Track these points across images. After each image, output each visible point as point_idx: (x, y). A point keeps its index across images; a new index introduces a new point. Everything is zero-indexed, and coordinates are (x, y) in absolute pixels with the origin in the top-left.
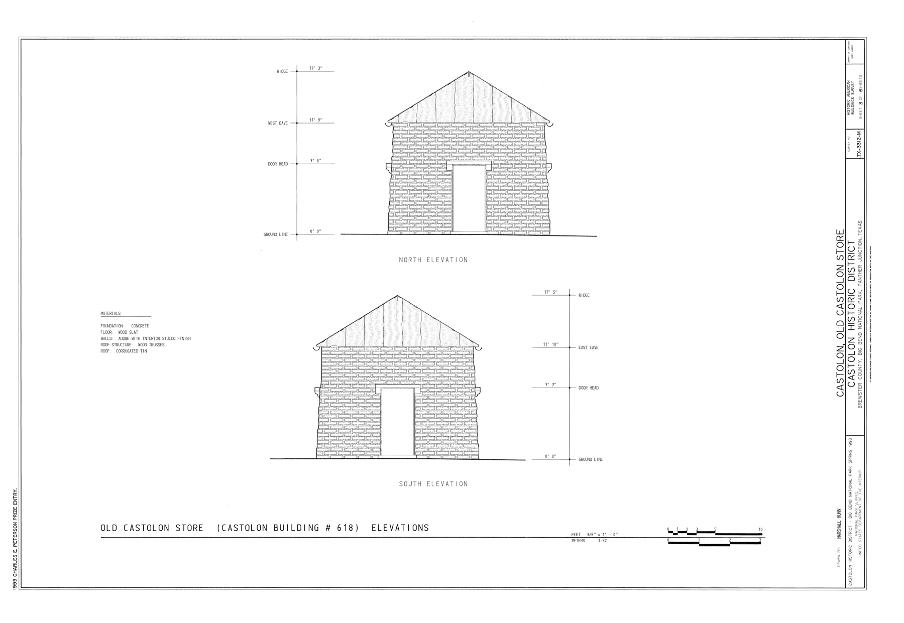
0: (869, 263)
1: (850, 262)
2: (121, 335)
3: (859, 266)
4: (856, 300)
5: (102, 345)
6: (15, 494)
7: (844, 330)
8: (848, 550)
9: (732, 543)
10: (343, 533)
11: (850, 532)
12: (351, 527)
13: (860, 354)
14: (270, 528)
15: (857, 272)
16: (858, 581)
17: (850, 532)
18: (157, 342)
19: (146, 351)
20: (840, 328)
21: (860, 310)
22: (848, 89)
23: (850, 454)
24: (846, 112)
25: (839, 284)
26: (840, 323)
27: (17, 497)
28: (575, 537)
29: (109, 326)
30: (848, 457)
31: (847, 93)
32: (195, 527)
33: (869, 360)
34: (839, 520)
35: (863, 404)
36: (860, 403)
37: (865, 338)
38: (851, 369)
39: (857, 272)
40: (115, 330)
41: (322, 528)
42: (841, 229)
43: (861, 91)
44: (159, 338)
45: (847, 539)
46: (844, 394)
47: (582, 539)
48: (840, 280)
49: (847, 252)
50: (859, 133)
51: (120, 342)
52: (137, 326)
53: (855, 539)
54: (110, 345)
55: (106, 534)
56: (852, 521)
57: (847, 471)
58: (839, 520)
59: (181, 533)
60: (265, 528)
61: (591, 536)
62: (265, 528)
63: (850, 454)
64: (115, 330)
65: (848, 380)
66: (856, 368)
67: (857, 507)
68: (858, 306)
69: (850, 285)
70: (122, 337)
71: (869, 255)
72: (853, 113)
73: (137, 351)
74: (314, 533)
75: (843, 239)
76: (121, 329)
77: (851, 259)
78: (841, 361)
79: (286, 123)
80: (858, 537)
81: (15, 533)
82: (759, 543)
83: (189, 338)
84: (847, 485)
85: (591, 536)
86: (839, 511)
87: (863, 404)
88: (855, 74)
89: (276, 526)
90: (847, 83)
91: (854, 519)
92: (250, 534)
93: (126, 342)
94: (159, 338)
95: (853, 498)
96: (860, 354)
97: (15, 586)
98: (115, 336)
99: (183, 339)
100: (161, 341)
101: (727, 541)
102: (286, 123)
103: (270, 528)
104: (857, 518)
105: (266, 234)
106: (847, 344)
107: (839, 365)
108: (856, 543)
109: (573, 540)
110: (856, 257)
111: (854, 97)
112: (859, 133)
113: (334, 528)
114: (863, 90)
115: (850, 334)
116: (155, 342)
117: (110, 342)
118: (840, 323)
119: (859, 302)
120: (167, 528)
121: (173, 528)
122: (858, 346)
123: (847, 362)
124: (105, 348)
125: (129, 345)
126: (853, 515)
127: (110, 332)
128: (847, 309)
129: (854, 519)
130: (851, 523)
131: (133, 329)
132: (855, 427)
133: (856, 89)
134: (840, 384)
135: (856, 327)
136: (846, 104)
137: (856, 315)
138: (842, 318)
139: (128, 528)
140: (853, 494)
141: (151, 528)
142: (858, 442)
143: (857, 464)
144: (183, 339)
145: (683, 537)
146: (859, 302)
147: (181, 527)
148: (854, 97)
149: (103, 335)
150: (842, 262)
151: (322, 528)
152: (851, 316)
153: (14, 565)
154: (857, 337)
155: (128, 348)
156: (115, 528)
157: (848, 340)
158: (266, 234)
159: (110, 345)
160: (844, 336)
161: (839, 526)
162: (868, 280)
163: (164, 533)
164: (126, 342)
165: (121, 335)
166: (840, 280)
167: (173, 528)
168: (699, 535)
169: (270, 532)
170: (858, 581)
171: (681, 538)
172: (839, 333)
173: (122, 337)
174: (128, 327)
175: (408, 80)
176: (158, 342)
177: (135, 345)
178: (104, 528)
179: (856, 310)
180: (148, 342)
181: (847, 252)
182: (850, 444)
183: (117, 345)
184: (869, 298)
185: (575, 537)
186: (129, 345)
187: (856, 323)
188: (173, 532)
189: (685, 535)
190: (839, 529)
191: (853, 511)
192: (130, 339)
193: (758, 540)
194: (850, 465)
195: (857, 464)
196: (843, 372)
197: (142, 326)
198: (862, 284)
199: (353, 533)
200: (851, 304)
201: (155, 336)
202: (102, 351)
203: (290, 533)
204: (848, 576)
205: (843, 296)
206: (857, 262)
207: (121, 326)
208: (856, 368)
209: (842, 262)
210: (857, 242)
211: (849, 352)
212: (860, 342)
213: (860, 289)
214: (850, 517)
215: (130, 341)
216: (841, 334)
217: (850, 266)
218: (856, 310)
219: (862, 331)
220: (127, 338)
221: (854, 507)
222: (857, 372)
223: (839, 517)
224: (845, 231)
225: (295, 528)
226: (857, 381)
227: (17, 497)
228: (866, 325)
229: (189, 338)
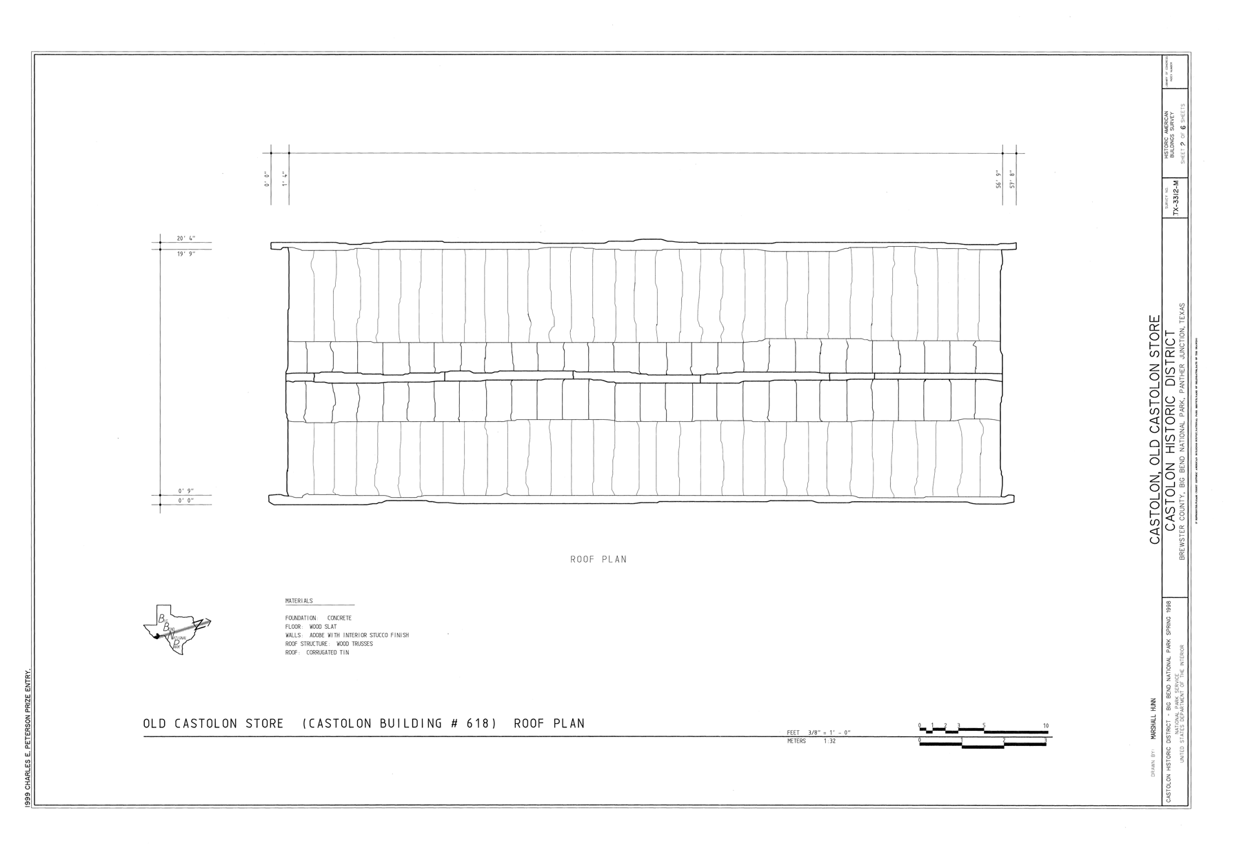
1: (1169, 359)
3: (1181, 366)
4: (1176, 412)
5: (287, 644)
6: (27, 677)
7: (1160, 453)
8: (1166, 754)
9: (1006, 744)
10: (475, 730)
11: (1168, 730)
12: (486, 722)
13: (1182, 485)
14: (376, 723)
15: (1177, 374)
16: (1179, 797)
17: (1168, 730)
18: (363, 640)
20: (1155, 451)
21: (1182, 426)
22: (1166, 122)
23: (1168, 622)
25: (1153, 389)
26: (1155, 444)
27: (30, 680)
28: (793, 737)
29: (296, 618)
30: (1165, 626)
31: (1164, 128)
33: (1194, 494)
34: (1153, 713)
35: (1186, 554)
37: (1189, 464)
38: (1170, 505)
39: (1177, 374)
40: (305, 624)
41: (446, 723)
43: (1183, 128)
44: (365, 635)
45: (1165, 739)
46: (1161, 540)
47: (801, 739)
48: (1155, 384)
49: (1165, 346)
50: (1176, 183)
51: (312, 639)
52: (335, 618)
53: (1175, 738)
54: (299, 644)
55: (150, 731)
56: (1171, 715)
57: (1165, 645)
58: (1153, 713)
59: (253, 731)
61: (814, 735)
62: (368, 723)
63: (1168, 622)
64: (305, 624)
66: (1177, 505)
67: (1178, 695)
68: (1179, 420)
69: (1169, 392)
71: (1194, 350)
72: (1172, 156)
74: (435, 731)
75: (1159, 328)
76: (313, 622)
78: (1155, 495)
81: (27, 730)
82: (1044, 744)
83: (407, 635)
84: (1165, 665)
85: (814, 735)
86: (1153, 702)
87: (1186, 554)
88: (1174, 102)
89: (383, 721)
91: (1174, 711)
93: (321, 640)
94: (365, 635)
95: (1172, 683)
96: (1182, 485)
97: (27, 803)
98: (305, 632)
99: (399, 635)
100: (368, 639)
101: (1000, 742)
103: (376, 723)
104: (1179, 710)
106: (1165, 472)
107: (1153, 500)
108: (1176, 744)
110: (1177, 353)
111: (1173, 134)
112: (1176, 183)
113: (462, 724)
114: (1187, 128)
115: (1168, 458)
116: (359, 639)
117: (299, 640)
118: (1155, 444)
119: (1181, 415)
121: (242, 724)
122: (1179, 475)
123: (1165, 497)
124: (292, 648)
125: (324, 644)
126: (1173, 706)
127: (299, 626)
129: (1174, 711)
130: (1170, 716)
131: (331, 623)
132: (1176, 586)
133: (1178, 123)
135: (1176, 449)
137: (1176, 433)
138: (1158, 436)
139: (181, 723)
140: (1172, 677)
142: (1179, 607)
143: (1178, 637)
144: (399, 635)
145: (939, 737)
148: (1173, 134)
149: (289, 631)
150: (1157, 360)
151: (446, 723)
152: (1169, 433)
153: (27, 774)
155: (323, 648)
157: (1165, 467)
159: (299, 644)
160: (1160, 461)
161: (1154, 721)
163: (230, 731)
164: (321, 640)
167: (242, 724)
168: (961, 733)
169: (376, 729)
170: (1179, 797)
171: (935, 737)
172: (1153, 456)
174: (322, 620)
176: (364, 639)
177: (332, 644)
178: (148, 723)
179: (1176, 426)
180: (350, 640)
181: (1165, 346)
182: (1169, 609)
183: (309, 644)
184: (1194, 409)
185: (793, 737)
186: (324, 644)
187: (1177, 442)
188: (242, 728)
189: (943, 733)
190: (1153, 726)
191: (1172, 700)
192: (326, 635)
193: (1042, 741)
194: (1168, 637)
195: (1178, 637)
196: (1159, 510)
197: (342, 618)
199: (489, 731)
200: (1170, 421)
201: (360, 631)
202: (287, 652)
204: (1165, 791)
205: (1159, 406)
206: (1178, 360)
207: (314, 618)
208: (1177, 505)
209: (1157, 360)
210: (1177, 333)
211: (1167, 483)
212: (1182, 470)
213: (1181, 397)
214: (1168, 709)
215: (326, 638)
216: (1156, 459)
217: (1169, 366)
220: (321, 635)
221: (1174, 695)
222: (1178, 510)
223: (1153, 709)
225: (409, 723)
226: (1178, 523)
227: (30, 680)
228: (1190, 447)
229: (407, 635)
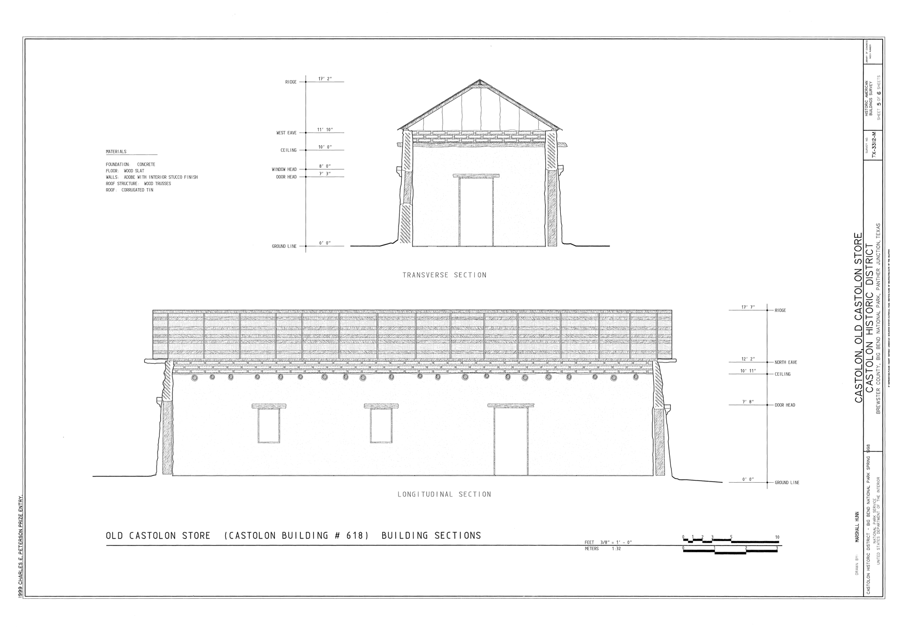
0: (887, 266)
1: (868, 265)
2: (127, 174)
3: (878, 270)
4: (874, 304)
5: (107, 183)
7: (862, 334)
8: (866, 558)
9: (748, 551)
10: (352, 541)
12: (361, 534)
13: (878, 359)
14: (279, 535)
15: (875, 276)
16: (876, 590)
18: (163, 181)
19: (152, 190)
20: (859, 333)
21: (878, 314)
22: (866, 90)
24: (864, 113)
27: (22, 501)
28: (589, 546)
29: (114, 164)
31: (865, 93)
32: (202, 535)
34: (857, 523)
35: (881, 409)
36: (878, 408)
37: (883, 342)
39: (875, 276)
40: (121, 169)
41: (331, 535)
42: (859, 232)
43: (879, 93)
44: (165, 177)
46: (863, 400)
47: (596, 547)
48: (859, 284)
50: (874, 134)
51: (125, 180)
52: (143, 164)
53: (873, 546)
55: (111, 542)
56: (871, 524)
57: (866, 478)
58: (857, 523)
59: (188, 541)
60: (273, 535)
61: (605, 544)
62: (273, 535)
64: (121, 169)
65: (866, 385)
66: (874, 373)
67: (876, 514)
68: (876, 310)
69: (868, 289)
70: (128, 176)
71: (887, 258)
72: (871, 114)
73: (143, 190)
76: (127, 167)
77: (869, 262)
78: (859, 366)
79: (294, 133)
80: (876, 544)
82: (776, 551)
83: (196, 177)
84: (866, 492)
85: (605, 544)
86: (857, 514)
87: (881, 409)
88: (873, 74)
89: (284, 534)
90: (865, 83)
91: (872, 526)
92: (258, 541)
93: (132, 180)
94: (165, 177)
95: (871, 505)
96: (878, 359)
97: (20, 594)
98: (121, 174)
99: (190, 177)
100: (167, 180)
101: (743, 549)
102: (294, 133)
103: (279, 535)
104: (876, 526)
105: (275, 246)
108: (874, 551)
109: (587, 548)
110: (874, 261)
111: (872, 98)
112: (874, 134)
113: (343, 536)
114: (882, 93)
117: (116, 181)
119: (877, 306)
120: (173, 535)
121: (179, 536)
122: (876, 351)
125: (134, 183)
126: (872, 522)
127: (116, 171)
128: (865, 313)
129: (872, 526)
131: (140, 168)
133: (875, 90)
134: (858, 307)
135: (874, 331)
136: (864, 104)
138: (860, 323)
139: (134, 535)
140: (871, 501)
141: (157, 536)
143: (875, 471)
144: (190, 177)
145: (698, 545)
146: (877, 306)
147: (188, 535)
148: (872, 98)
149: (108, 174)
150: (860, 266)
151: (331, 535)
152: (869, 320)
153: (20, 573)
154: (875, 342)
155: (134, 187)
156: (120, 535)
157: (866, 345)
158: (275, 246)
159: (116, 184)
160: (862, 341)
161: (857, 529)
162: (887, 284)
163: (171, 541)
164: (132, 180)
165: (127, 174)
166: (859, 284)
167: (179, 536)
168: (714, 543)
169: (279, 540)
170: (876, 590)
171: (696, 546)
172: (857, 337)
173: (128, 176)
174: (133, 166)
175: (418, 81)
176: (164, 180)
177: (140, 183)
178: (109, 535)
179: (874, 314)
180: (154, 180)
183: (123, 183)
185: (589, 546)
186: (134, 183)
187: (874, 327)
188: (179, 539)
189: (700, 543)
190: (857, 533)
191: (871, 518)
192: (136, 177)
193: (775, 548)
194: (868, 471)
195: (875, 471)
197: (148, 164)
198: (881, 288)
199: (363, 541)
201: (161, 174)
202: (107, 190)
203: (298, 541)
204: (866, 585)
206: (875, 266)
207: (127, 164)
208: (874, 373)
210: (875, 245)
212: (878, 348)
214: (868, 524)
215: (136, 180)
216: (860, 339)
217: (869, 270)
218: (874, 314)
219: (880, 335)
220: (132, 177)
221: (872, 514)
222: (875, 377)
223: (857, 520)
224: (863, 234)
225: (303, 536)
226: (875, 386)
227: (22, 501)
228: (885, 329)
229: (196, 177)
